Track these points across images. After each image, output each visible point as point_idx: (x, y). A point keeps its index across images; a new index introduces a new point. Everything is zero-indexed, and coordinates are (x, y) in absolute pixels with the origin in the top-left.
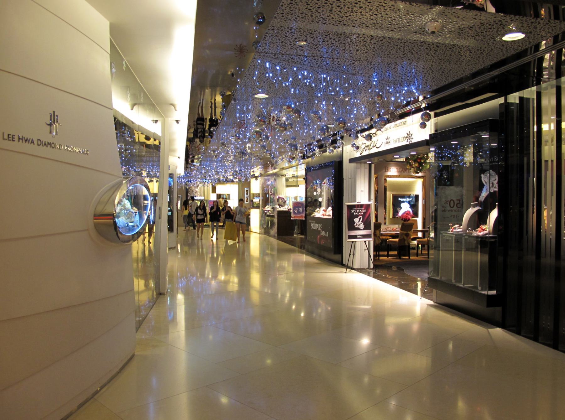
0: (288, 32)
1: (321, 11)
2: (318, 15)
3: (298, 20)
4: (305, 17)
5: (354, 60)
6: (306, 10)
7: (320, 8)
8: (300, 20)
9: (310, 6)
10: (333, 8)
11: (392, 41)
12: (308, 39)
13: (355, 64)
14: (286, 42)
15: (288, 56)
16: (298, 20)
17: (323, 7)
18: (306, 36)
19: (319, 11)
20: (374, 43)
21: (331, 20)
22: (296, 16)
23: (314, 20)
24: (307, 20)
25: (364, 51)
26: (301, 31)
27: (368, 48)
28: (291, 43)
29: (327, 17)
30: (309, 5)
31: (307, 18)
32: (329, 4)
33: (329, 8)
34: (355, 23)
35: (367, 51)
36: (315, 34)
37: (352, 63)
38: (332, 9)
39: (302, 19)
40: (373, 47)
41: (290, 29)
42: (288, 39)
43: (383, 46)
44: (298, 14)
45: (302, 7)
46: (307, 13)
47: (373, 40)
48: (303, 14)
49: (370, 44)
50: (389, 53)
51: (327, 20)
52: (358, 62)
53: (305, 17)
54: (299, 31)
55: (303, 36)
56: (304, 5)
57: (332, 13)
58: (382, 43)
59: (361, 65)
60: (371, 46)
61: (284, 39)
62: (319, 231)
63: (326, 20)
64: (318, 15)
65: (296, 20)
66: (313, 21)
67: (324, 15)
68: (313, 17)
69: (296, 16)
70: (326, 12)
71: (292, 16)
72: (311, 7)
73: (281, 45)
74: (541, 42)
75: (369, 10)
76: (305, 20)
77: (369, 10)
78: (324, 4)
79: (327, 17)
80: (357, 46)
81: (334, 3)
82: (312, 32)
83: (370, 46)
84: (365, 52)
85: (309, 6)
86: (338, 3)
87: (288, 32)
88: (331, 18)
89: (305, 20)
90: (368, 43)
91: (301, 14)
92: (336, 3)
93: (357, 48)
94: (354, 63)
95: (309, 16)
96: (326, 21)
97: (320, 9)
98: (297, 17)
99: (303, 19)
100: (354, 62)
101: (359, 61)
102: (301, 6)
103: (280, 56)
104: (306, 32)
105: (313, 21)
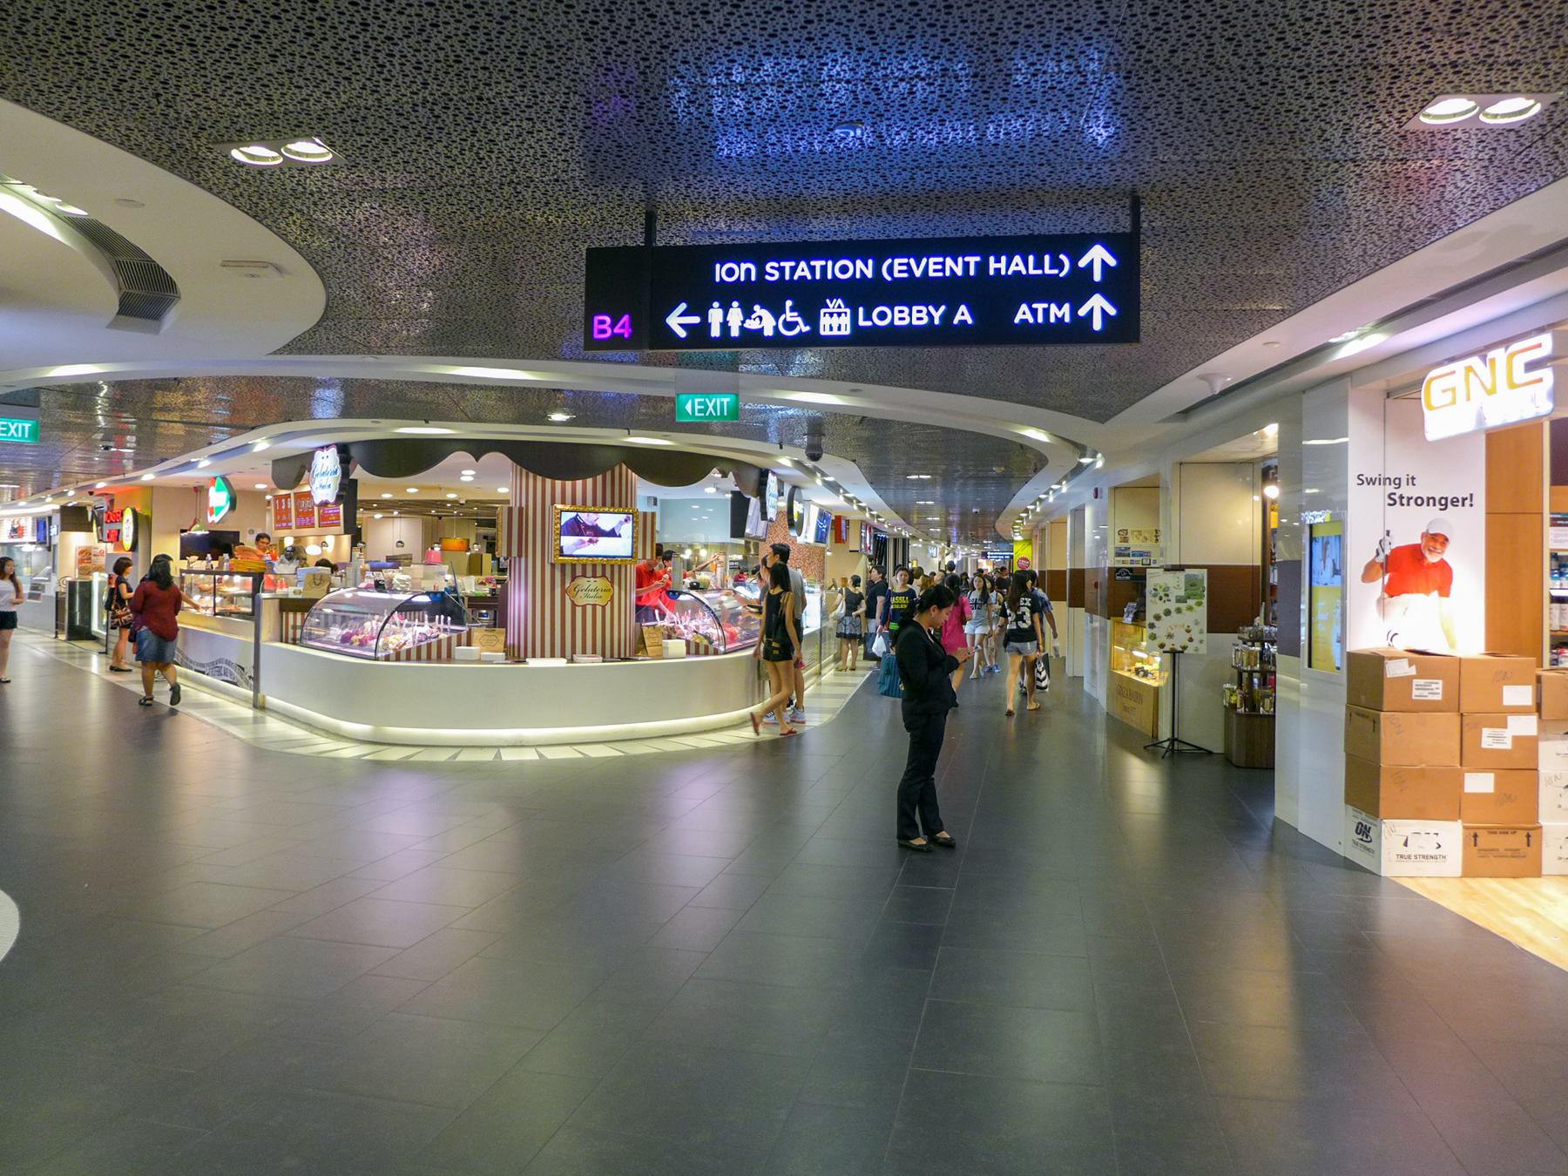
0: (1098, 134)
1: (1181, 61)
2: (1149, 125)
3: (1144, 38)
4: (1139, 85)
5: (1337, 162)
6: (1115, 117)
7: (1175, 51)
8: (1153, 37)
9: (1146, 50)
10: (1215, 47)
11: (1467, 78)
12: (1184, 106)
13: (1339, 174)
14: (1085, 200)
15: (1127, 166)
16: (1144, 38)
17: (1186, 47)
18: (1209, 38)
19: (1175, 61)
20: (1404, 97)
21: (1252, 20)
22: (1138, 26)
23: (1194, 31)
24: (1173, 33)
25: (1369, 127)
26: (1134, 130)
27: (1381, 118)
28: (1133, 126)
29: (1235, 14)
30: (1143, 47)
31: (1121, 135)
32: (1202, 38)
33: (1204, 49)
34: (1322, 47)
35: (1302, 201)
36: (1240, 22)
37: (1422, 79)
38: (1212, 50)
39: (1156, 34)
40: (1401, 112)
41: (1125, 78)
42: (1105, 155)
43: (1383, 147)
44: (1140, 16)
45: (1125, 57)
46: (1141, 74)
47: (1350, 134)
48: (1130, 78)
49: (1343, 145)
50: (1430, 154)
51: (1176, 135)
52: (1351, 164)
53: (1139, 85)
54: (1131, 130)
55: (1168, 96)
56: (1129, 49)
57: (1181, 118)
58: (1380, 140)
59: (1323, 208)
60: (1394, 107)
61: (1064, 223)
62: (1280, 651)
63: (1198, 89)
64: (1149, 125)
65: (1113, 97)
66: (1192, 36)
67: (1163, 124)
68: (1192, 22)
69: (1078, 174)
70: (1194, 62)
71: (1125, 28)
72: (1126, 108)
73: (1126, 87)
74: (1105, 464)
75: (1329, 32)
76: (1167, 36)
77: (1329, 32)
78: (1185, 39)
79: (1235, 14)
80: (1271, 191)
81: (1215, 32)
82: (1167, 129)
83: (1344, 151)
84: (1371, 130)
85: (1144, 52)
86: (1226, 30)
87: (1098, 134)
88: (1251, 13)
89: (1167, 36)
90: (1337, 144)
91: (1151, 15)
92: (1187, 92)
93: (1346, 120)
94: (1336, 171)
95: (1150, 81)
96: (1234, 30)
97: (1176, 55)
98: (1140, 30)
99: (1161, 34)
100: (1336, 166)
101: (1353, 160)
102: (1121, 55)
103: (1106, 168)
104: (1209, 18)
105: (1192, 36)
